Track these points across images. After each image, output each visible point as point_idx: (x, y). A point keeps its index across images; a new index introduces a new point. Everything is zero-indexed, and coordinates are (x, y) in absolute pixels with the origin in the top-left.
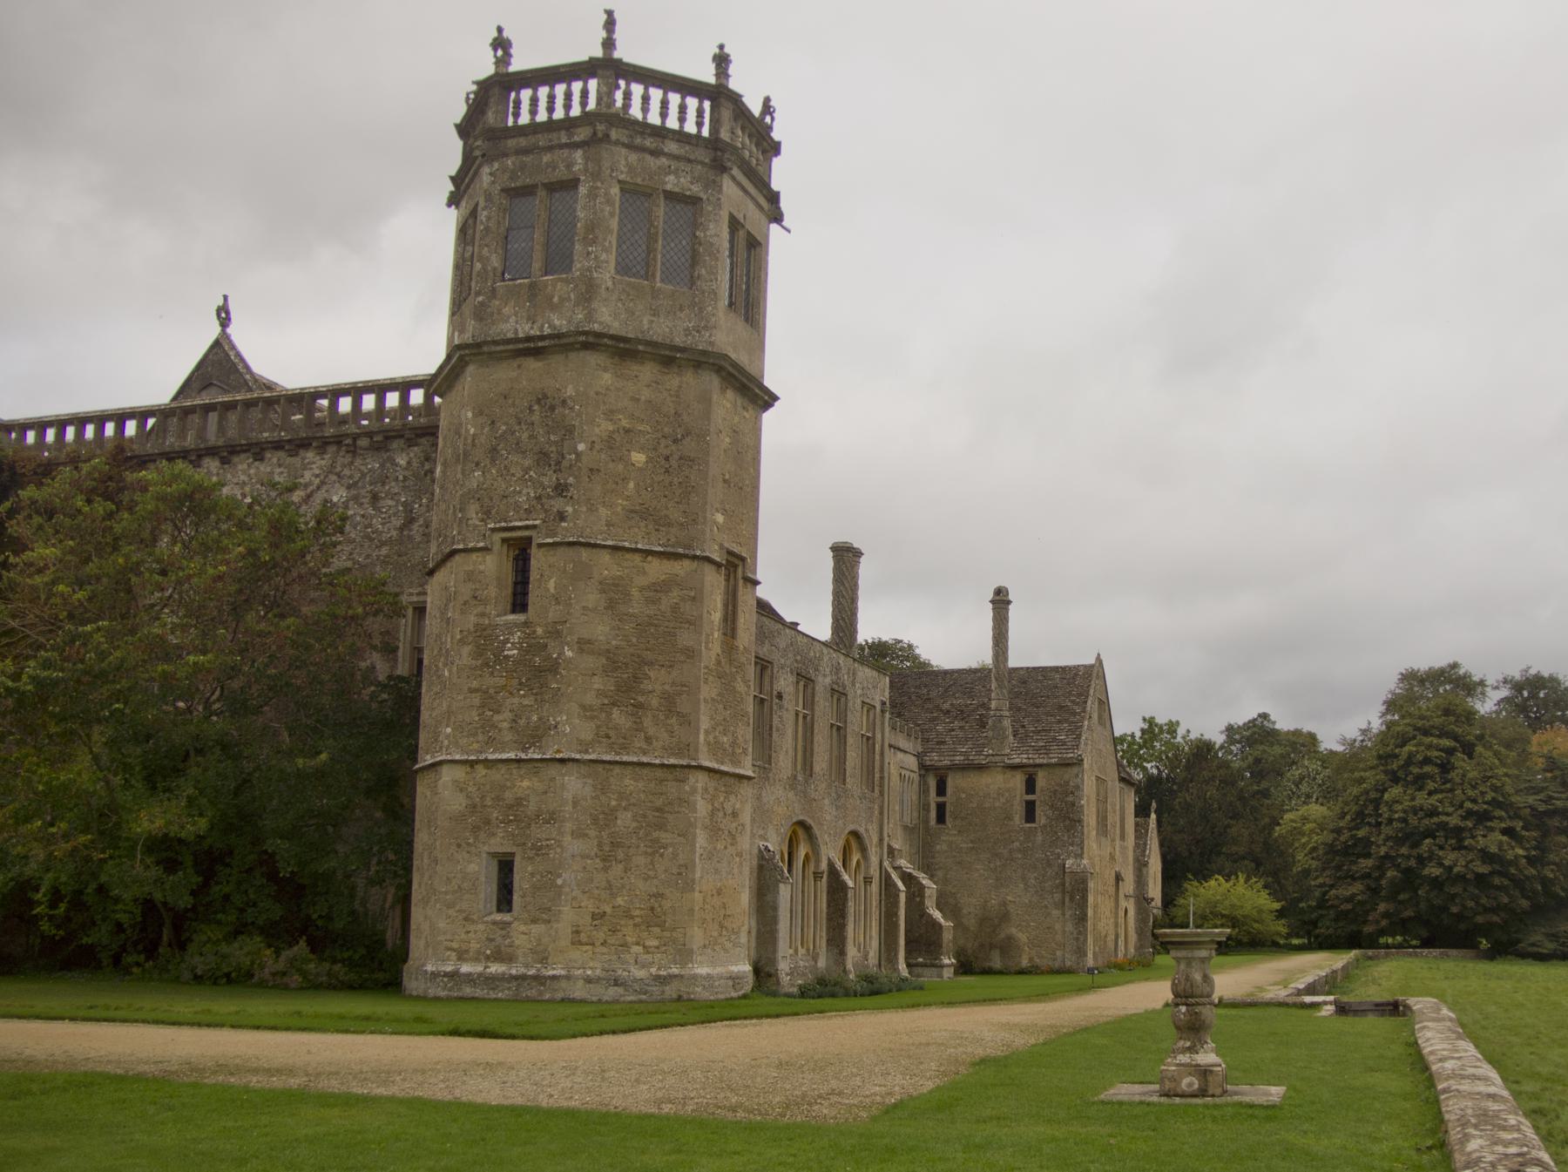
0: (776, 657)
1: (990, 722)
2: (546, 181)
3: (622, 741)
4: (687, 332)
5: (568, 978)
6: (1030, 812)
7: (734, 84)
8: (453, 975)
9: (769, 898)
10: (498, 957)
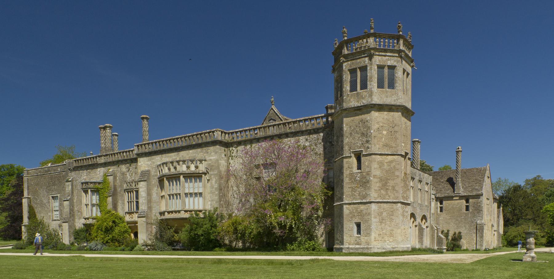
2: (359, 66)
3: (384, 197)
4: (395, 100)
5: (374, 248)
6: (467, 208)
8: (348, 248)
10: (358, 244)
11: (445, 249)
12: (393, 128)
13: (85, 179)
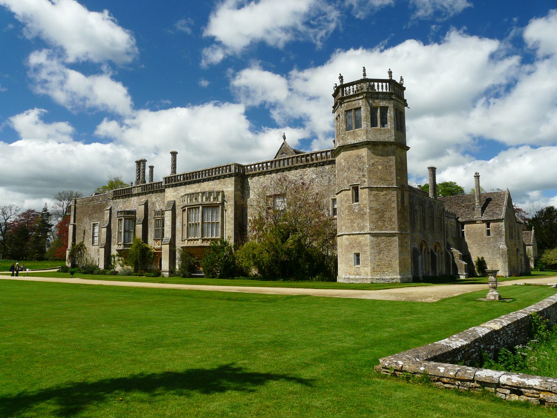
1: (476, 209)
6: (488, 233)
7: (393, 78)
10: (357, 274)
12: (388, 162)
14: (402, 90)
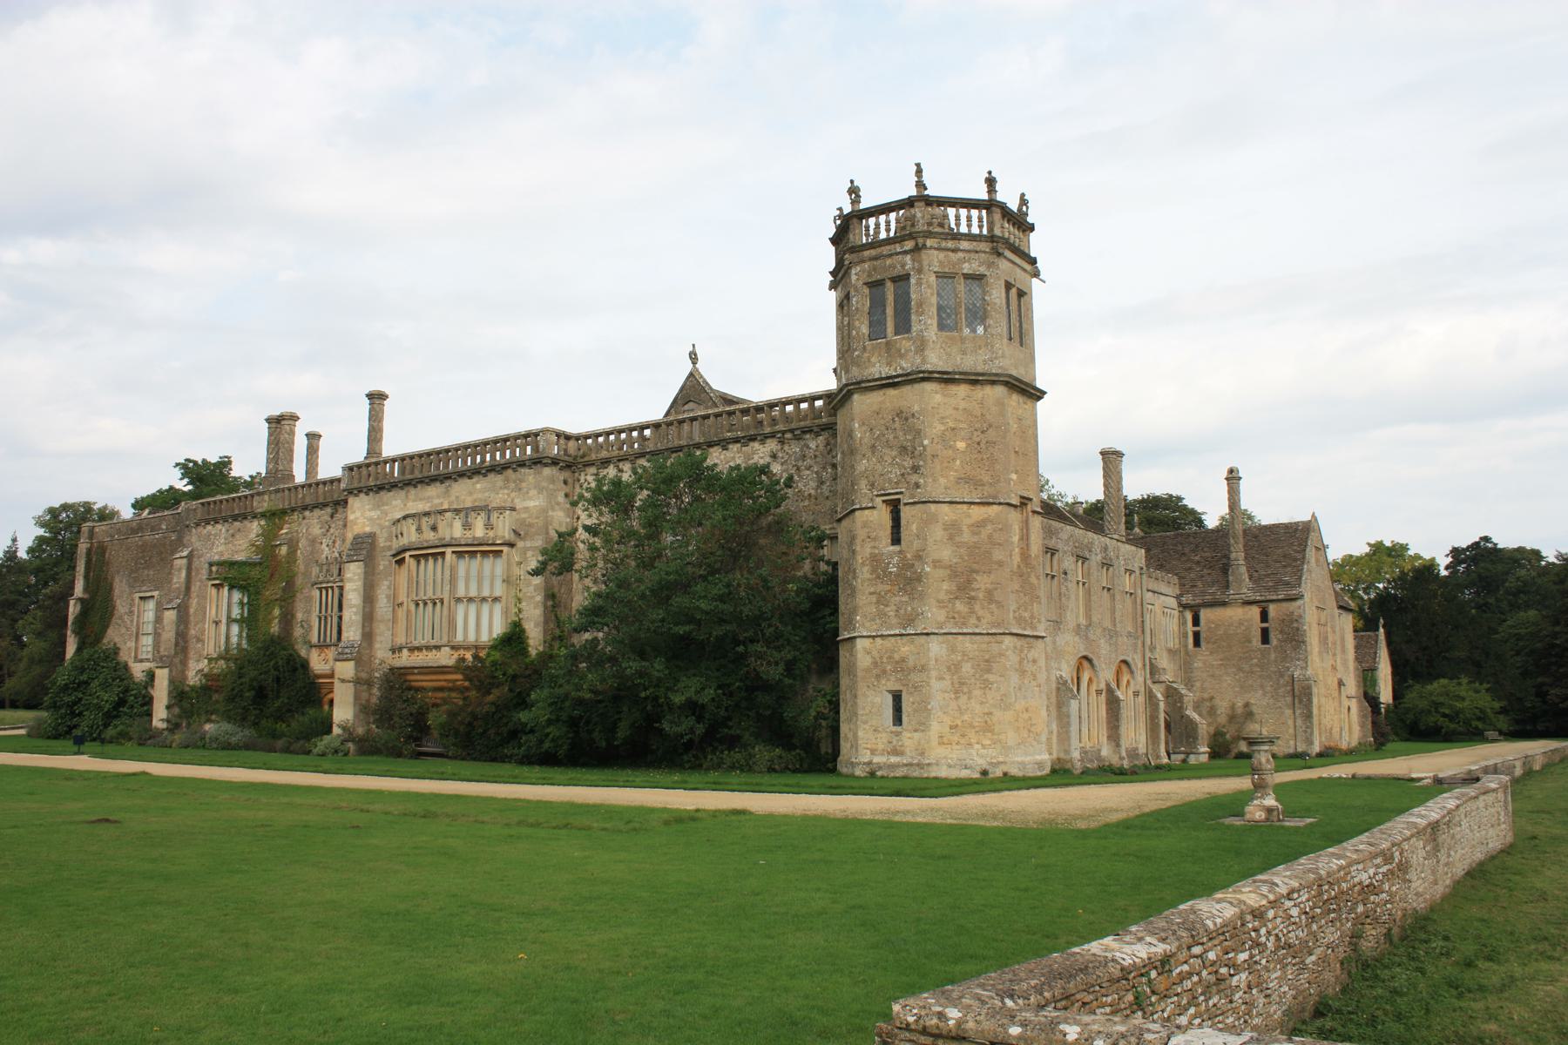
0: (1060, 546)
6: (1265, 636)
7: (1000, 197)
9: (1064, 710)
11: (1204, 753)
13: (221, 554)
14: (1024, 231)
